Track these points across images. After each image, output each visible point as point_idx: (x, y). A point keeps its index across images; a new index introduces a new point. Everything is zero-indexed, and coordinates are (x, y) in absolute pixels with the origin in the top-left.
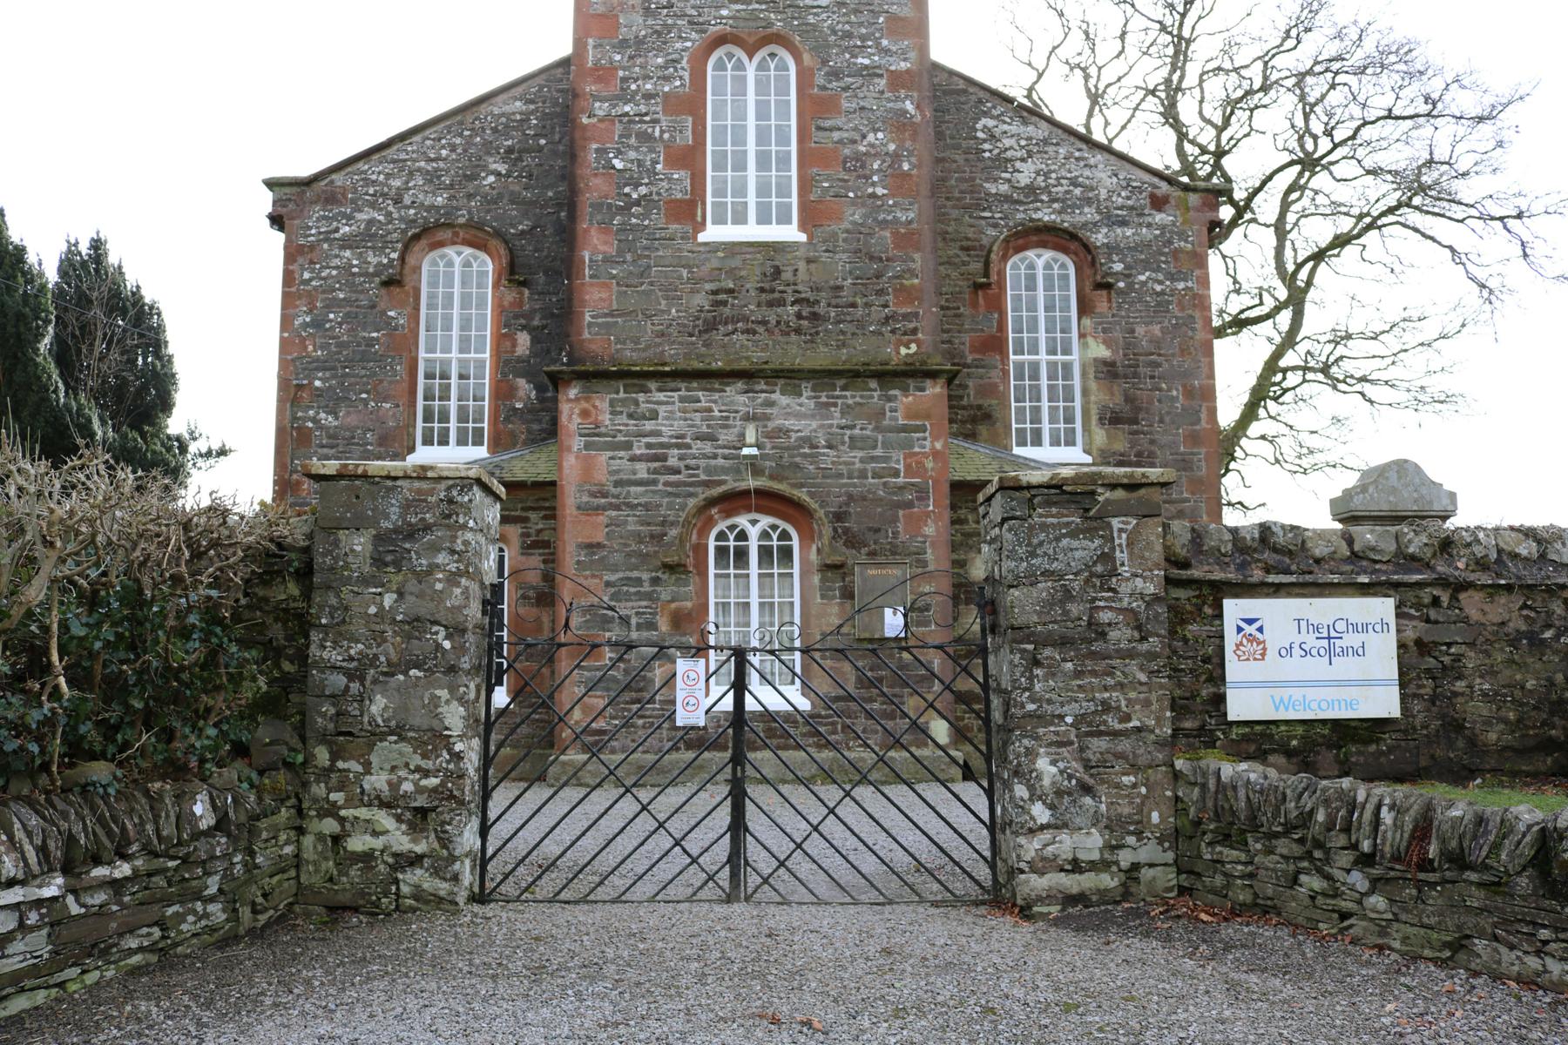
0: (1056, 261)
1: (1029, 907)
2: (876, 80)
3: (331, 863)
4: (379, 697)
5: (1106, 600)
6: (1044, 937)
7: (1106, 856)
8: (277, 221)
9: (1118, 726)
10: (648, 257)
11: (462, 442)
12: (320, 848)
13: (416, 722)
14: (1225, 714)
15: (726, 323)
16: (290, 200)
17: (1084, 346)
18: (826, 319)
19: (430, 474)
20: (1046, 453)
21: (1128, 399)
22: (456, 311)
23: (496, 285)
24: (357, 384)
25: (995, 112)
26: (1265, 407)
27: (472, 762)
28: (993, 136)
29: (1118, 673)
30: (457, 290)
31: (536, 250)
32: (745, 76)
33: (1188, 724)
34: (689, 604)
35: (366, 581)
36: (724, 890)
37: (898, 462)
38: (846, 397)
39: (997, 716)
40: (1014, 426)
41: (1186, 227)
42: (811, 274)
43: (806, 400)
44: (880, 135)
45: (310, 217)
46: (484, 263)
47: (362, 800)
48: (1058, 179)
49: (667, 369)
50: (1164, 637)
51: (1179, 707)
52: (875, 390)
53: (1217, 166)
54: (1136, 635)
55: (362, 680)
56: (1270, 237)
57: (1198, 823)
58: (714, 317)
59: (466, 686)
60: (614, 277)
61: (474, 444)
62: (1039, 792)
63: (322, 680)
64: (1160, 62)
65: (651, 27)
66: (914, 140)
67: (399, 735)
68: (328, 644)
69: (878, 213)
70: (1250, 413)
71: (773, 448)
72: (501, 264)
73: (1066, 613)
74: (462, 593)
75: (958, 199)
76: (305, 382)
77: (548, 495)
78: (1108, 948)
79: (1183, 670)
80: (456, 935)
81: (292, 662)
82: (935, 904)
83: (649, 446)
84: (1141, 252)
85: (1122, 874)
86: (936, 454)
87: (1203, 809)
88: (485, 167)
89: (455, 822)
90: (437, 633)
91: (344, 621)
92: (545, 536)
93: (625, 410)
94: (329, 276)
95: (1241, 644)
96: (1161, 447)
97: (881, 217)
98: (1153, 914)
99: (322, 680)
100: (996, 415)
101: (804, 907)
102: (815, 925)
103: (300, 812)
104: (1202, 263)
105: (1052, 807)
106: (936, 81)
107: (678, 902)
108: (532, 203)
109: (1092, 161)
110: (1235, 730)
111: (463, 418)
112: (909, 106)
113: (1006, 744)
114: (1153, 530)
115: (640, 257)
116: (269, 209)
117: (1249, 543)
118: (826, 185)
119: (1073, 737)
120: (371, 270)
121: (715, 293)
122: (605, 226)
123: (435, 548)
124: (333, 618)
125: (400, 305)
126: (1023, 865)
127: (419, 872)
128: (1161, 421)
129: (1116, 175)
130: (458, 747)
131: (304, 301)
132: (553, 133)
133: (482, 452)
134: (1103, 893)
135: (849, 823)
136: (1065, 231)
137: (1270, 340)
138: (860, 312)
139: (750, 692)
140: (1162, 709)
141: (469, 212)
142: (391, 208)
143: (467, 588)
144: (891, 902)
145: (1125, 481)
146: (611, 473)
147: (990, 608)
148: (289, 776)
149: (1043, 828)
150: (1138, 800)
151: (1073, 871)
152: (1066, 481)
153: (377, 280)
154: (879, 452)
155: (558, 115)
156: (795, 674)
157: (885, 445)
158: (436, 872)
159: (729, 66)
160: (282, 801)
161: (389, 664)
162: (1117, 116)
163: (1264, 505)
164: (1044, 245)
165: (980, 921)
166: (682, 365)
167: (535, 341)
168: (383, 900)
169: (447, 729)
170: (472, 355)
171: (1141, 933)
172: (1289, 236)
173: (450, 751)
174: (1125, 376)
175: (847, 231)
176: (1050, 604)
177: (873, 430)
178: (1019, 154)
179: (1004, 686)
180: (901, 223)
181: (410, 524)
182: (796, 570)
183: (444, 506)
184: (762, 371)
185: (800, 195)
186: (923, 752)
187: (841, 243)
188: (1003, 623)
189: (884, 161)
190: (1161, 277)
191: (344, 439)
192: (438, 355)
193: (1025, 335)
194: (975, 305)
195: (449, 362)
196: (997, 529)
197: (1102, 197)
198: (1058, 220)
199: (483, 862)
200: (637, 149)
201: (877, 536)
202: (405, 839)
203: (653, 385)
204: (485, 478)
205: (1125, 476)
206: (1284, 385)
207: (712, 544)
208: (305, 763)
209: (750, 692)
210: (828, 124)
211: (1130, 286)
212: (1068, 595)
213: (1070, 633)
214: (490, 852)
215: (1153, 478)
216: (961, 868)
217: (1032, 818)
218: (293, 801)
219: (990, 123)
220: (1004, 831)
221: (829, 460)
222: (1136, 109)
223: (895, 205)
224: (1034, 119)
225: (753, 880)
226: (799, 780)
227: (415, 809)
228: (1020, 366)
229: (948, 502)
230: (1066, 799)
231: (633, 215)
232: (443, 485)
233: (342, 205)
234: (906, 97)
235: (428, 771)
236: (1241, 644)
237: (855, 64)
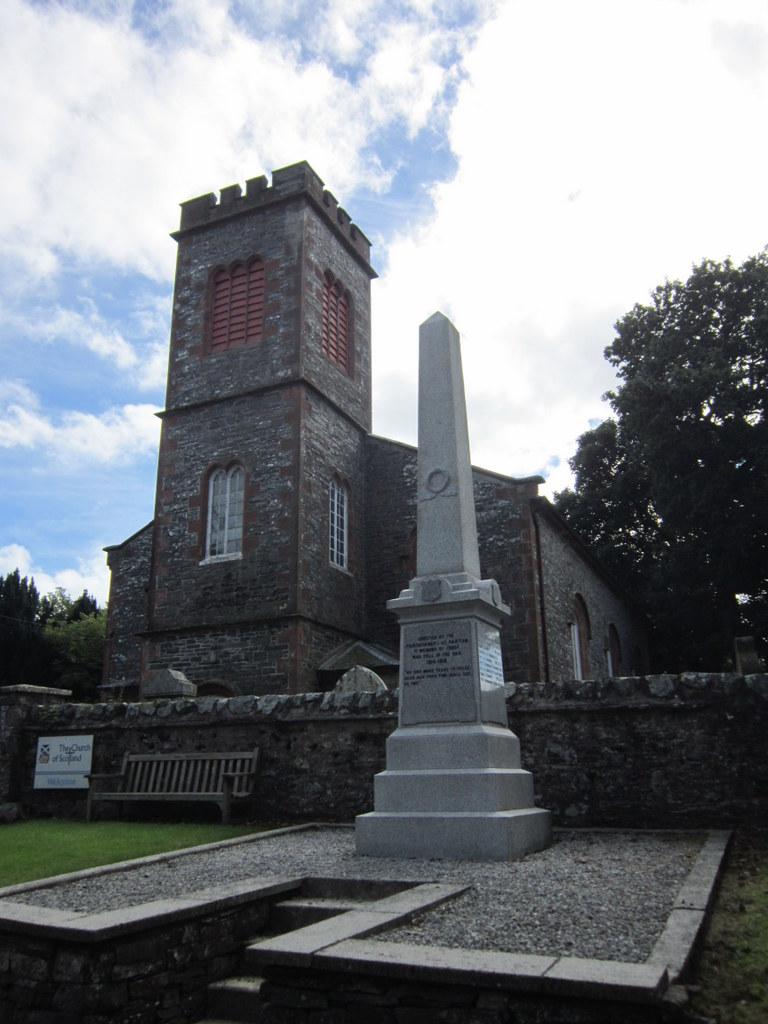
18: (248, 596)
43: (237, 639)
97: (275, 541)
121: (205, 589)
190: (502, 537)
210: (254, 500)
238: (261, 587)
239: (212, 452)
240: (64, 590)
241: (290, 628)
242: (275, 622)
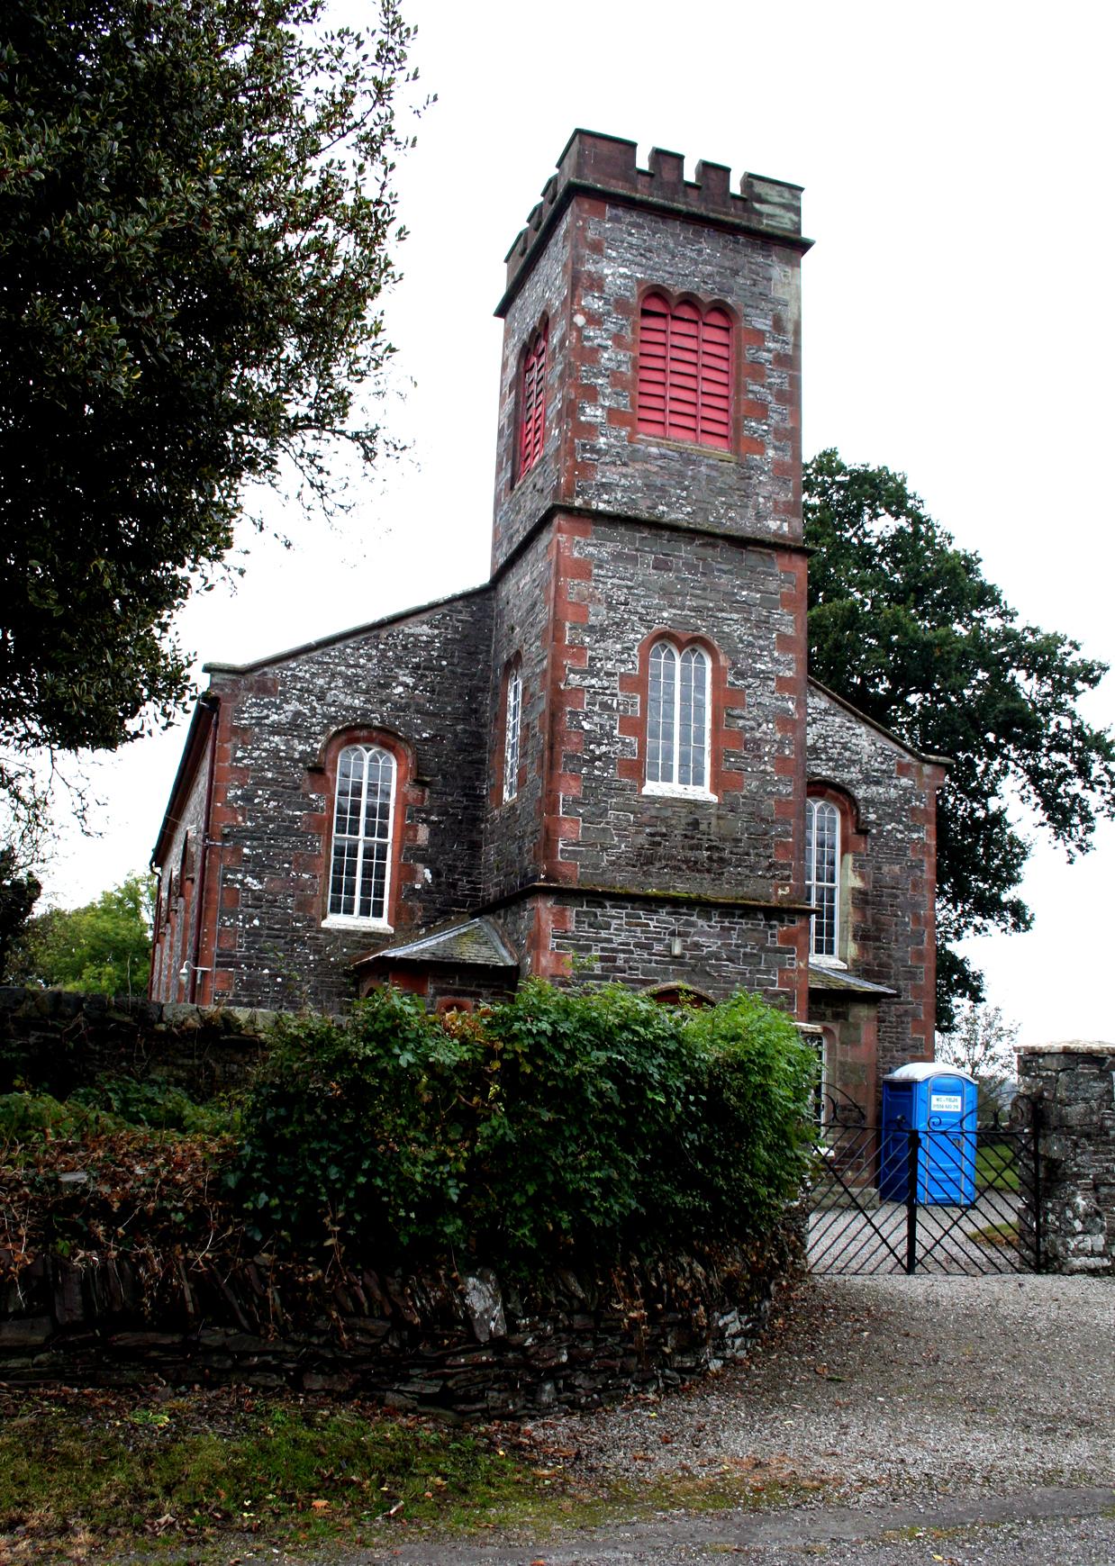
2: (770, 683)
21: (875, 922)
44: (771, 726)
46: (388, 760)
60: (580, 815)
83: (603, 949)
94: (260, 757)
105: (1083, 1222)
108: (434, 715)
109: (858, 731)
115: (600, 801)
121: (652, 835)
132: (452, 657)
141: (381, 716)
142: (315, 704)
167: (433, 834)
170: (376, 839)
174: (873, 903)
175: (744, 797)
190: (901, 827)
210: (736, 712)
211: (880, 832)
223: (779, 780)
224: (820, 693)
238: (748, 854)
239: (661, 610)
240: (1015, 926)
241: (798, 924)
242: (774, 913)
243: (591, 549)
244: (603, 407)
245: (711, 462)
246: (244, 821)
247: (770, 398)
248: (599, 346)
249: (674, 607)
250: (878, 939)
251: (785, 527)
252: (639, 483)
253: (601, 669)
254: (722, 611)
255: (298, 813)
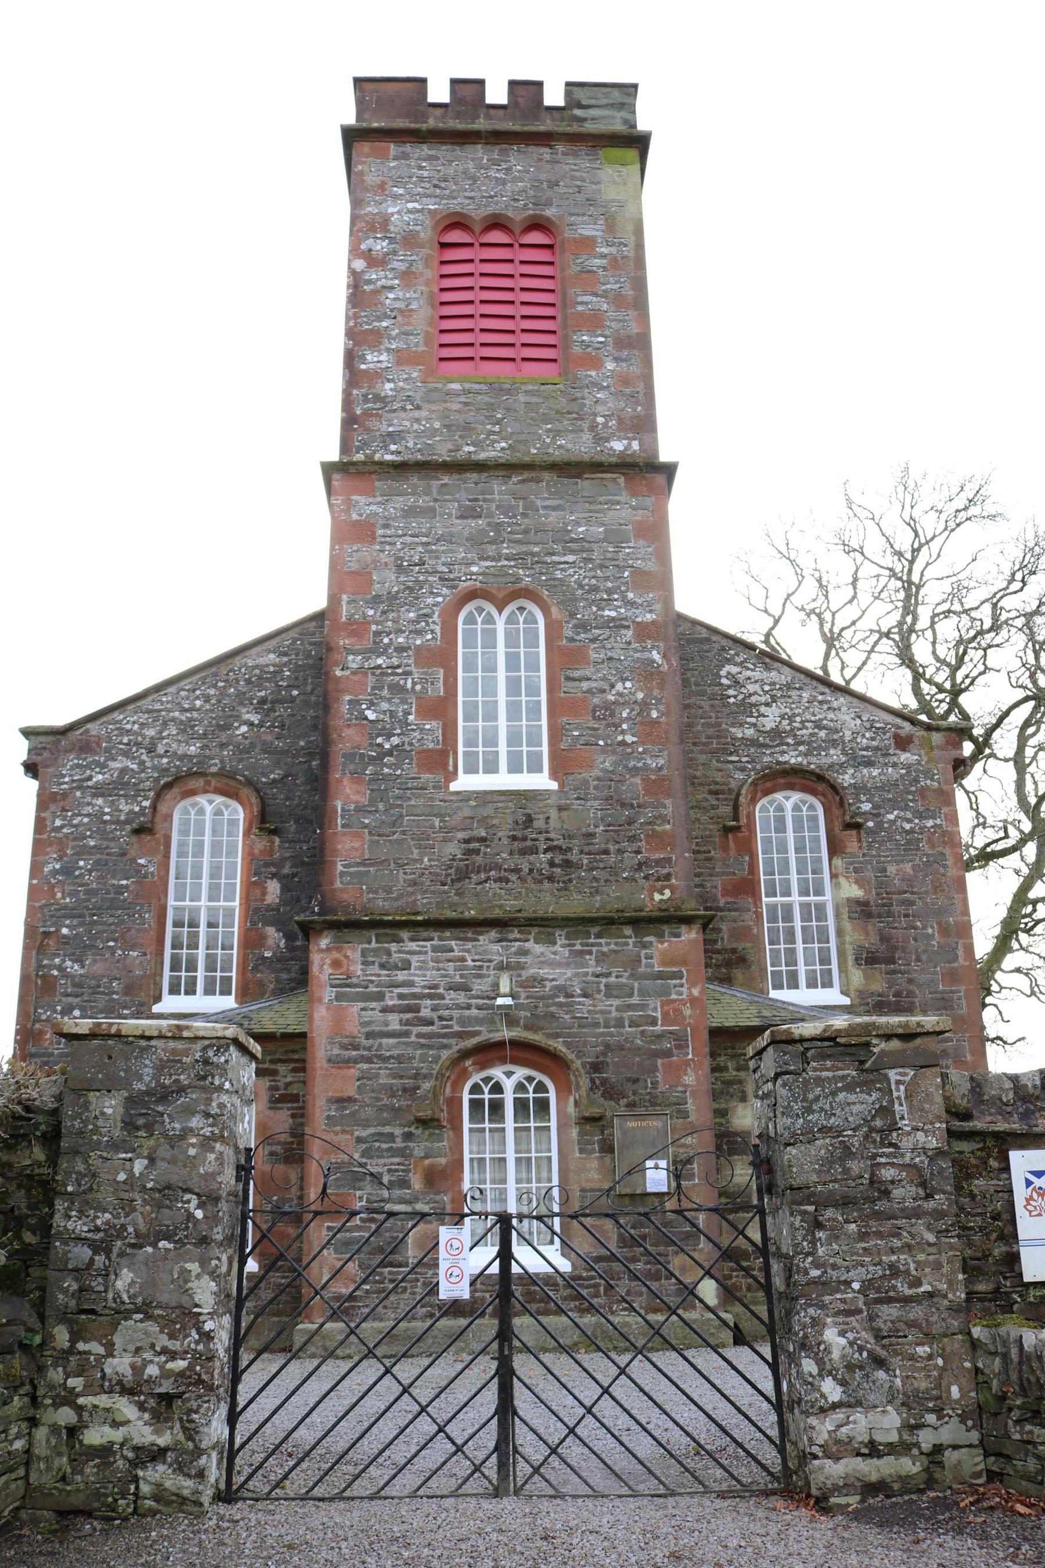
0: (804, 802)
1: (826, 1498)
2: (623, 632)
3: (65, 1459)
4: (125, 1271)
5: (887, 1156)
6: (846, 1535)
7: (905, 1437)
8: (31, 768)
9: (908, 1292)
10: (401, 806)
11: (209, 991)
12: (53, 1442)
13: (164, 1298)
14: (1021, 1275)
15: (479, 872)
16: (45, 748)
17: (837, 886)
19: (185, 1034)
20: (803, 996)
21: (884, 939)
22: (206, 860)
23: (247, 833)
24: (105, 931)
25: (738, 659)
26: (1018, 940)
27: (222, 1341)
28: (737, 682)
29: (905, 1234)
30: (207, 838)
31: (287, 799)
32: (495, 630)
33: (981, 1287)
34: (443, 1161)
35: (115, 1146)
36: (490, 1482)
37: (655, 1009)
38: (600, 945)
39: (778, 1282)
40: (769, 969)
41: (931, 766)
42: (563, 822)
43: (560, 948)
44: (628, 684)
45: (64, 765)
47: (102, 1386)
48: (802, 722)
49: (420, 918)
50: (951, 1194)
51: (972, 1269)
52: (630, 937)
53: (954, 704)
54: (921, 1192)
55: (108, 1252)
56: (1009, 772)
57: (1002, 1398)
58: (467, 866)
59: (219, 1259)
60: (366, 826)
61: (222, 993)
62: (828, 1367)
63: (66, 1253)
64: (892, 606)
65: (403, 583)
66: (661, 689)
67: (146, 1313)
68: (74, 1213)
69: (628, 760)
70: (1003, 945)
71: (528, 997)
72: (252, 812)
73: (846, 1171)
74: (217, 1159)
75: (705, 744)
76: (52, 929)
77: (297, 1047)
78: (918, 1548)
79: (971, 1228)
80: (200, 1544)
81: (34, 1233)
82: (722, 1495)
83: (401, 996)
84: (889, 791)
85: (923, 1457)
86: (693, 1001)
87: (1007, 1382)
88: (238, 718)
89: (202, 1411)
90: (188, 1202)
91: (91, 1189)
92: (294, 1090)
93: (377, 960)
94: (81, 824)
95: (1031, 1198)
96: (920, 986)
97: (631, 764)
98: (962, 1504)
99: (66, 1253)
100: (751, 957)
101: (580, 1501)
102: (593, 1525)
103: (34, 1400)
104: (949, 800)
105: (843, 1383)
106: (680, 630)
107: (442, 1497)
108: (284, 752)
109: (835, 704)
110: (1032, 1292)
111: (211, 966)
112: (656, 656)
113: (789, 1313)
114: (932, 1081)
115: (392, 806)
116: (24, 757)
117: (1031, 1091)
118: (576, 733)
119: (861, 1305)
120: (123, 818)
121: (467, 841)
122: (357, 776)
123: (189, 1111)
124: (79, 1185)
125: (150, 853)
126: (815, 1449)
127: (161, 1468)
128: (918, 960)
129: (859, 717)
130: (209, 1326)
131: (54, 848)
132: (305, 683)
133: (229, 1002)
134: (904, 1479)
135: (618, 1398)
136: (812, 773)
137: (1017, 872)
138: (612, 859)
139: (517, 1262)
140: (953, 1272)
141: (222, 762)
142: (144, 757)
143: (221, 1153)
144: (673, 1494)
145: (900, 1031)
146: (363, 1024)
147: (764, 1166)
148: (25, 1359)
149: (835, 1406)
150: (935, 1373)
151: (870, 1455)
152: (839, 1033)
153: (128, 827)
154: (635, 1000)
155: (311, 667)
156: (554, 1233)
157: (643, 993)
158: (180, 1468)
159: (479, 620)
160: (16, 1388)
161: (138, 1235)
162: (852, 658)
163: (1023, 1039)
164: (791, 787)
165: (773, 1516)
166: (435, 914)
167: (285, 889)
168: (120, 1502)
169: (197, 1306)
171: (954, 1530)
172: (1029, 770)
173: (199, 1331)
174: (880, 916)
175: (598, 779)
176: (829, 1162)
177: (629, 978)
178: (763, 699)
179: (784, 1250)
180: (652, 770)
181: (164, 1086)
182: (553, 1124)
183: (199, 1067)
184: (515, 919)
185: (551, 744)
186: (689, 1315)
187: (592, 790)
188: (781, 1183)
189: (633, 710)
190: (909, 815)
191: (89, 987)
192: (187, 903)
193: (777, 877)
194: (725, 848)
195: (199, 909)
196: (770, 1084)
197: (847, 738)
198: (805, 762)
199: (231, 1453)
200: (389, 700)
201: (635, 1087)
202: (147, 1430)
203: (405, 935)
204: (243, 1038)
205: (900, 1025)
206: (1035, 916)
207: (466, 1097)
208: (42, 1345)
209: (517, 1262)
210: (577, 674)
211: (879, 825)
212: (847, 1152)
213: (851, 1193)
214: (238, 1441)
215: (929, 1027)
216: (745, 1450)
217: (823, 1396)
218: (27, 1388)
219: (734, 670)
220: (792, 1411)
221: (585, 1009)
222: (872, 651)
223: (644, 752)
224: (777, 665)
225: (523, 1469)
226: (563, 1349)
227: (160, 1395)
228: (773, 908)
229: (707, 1050)
230: (858, 1374)
231: (385, 765)
232: (199, 1045)
233: (96, 753)
234: (653, 647)
235: (175, 1353)
236: (1031, 1198)
237: (602, 616)
239: (469, 564)
243: (373, 508)
244: (388, 350)
245: (530, 387)
246: (64, 898)
247: (605, 307)
248: (383, 287)
249: (486, 559)
250: (892, 961)
251: (635, 445)
252: (437, 425)
253: (388, 645)
254: (553, 554)
255: (124, 882)
